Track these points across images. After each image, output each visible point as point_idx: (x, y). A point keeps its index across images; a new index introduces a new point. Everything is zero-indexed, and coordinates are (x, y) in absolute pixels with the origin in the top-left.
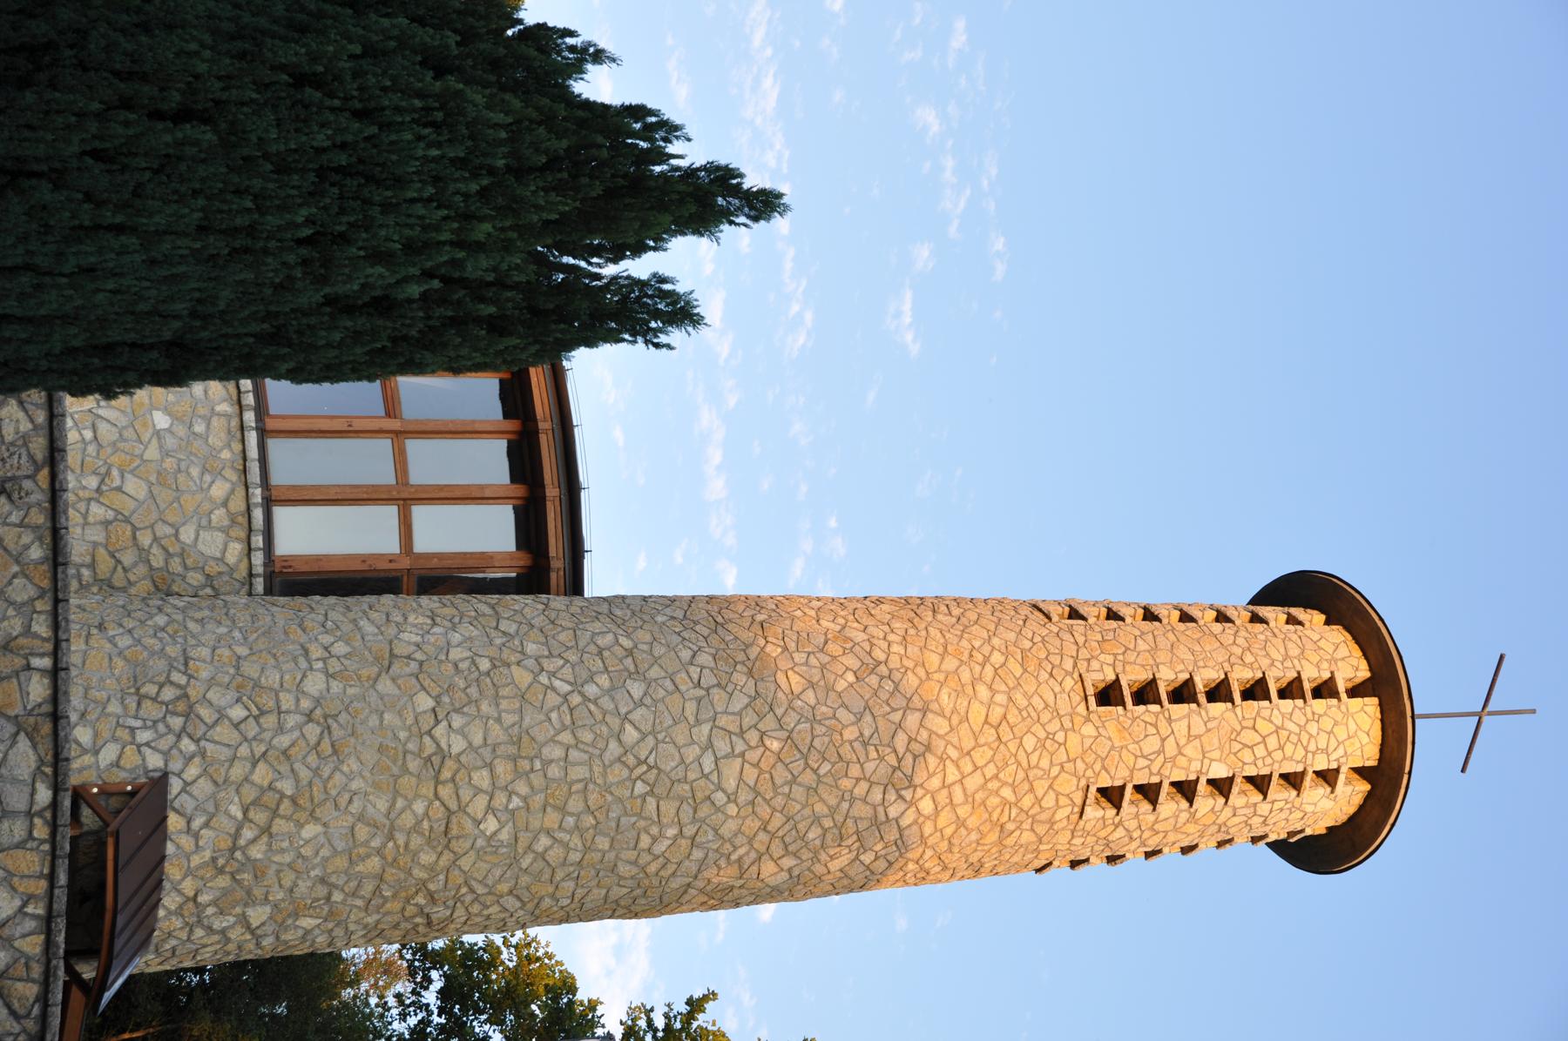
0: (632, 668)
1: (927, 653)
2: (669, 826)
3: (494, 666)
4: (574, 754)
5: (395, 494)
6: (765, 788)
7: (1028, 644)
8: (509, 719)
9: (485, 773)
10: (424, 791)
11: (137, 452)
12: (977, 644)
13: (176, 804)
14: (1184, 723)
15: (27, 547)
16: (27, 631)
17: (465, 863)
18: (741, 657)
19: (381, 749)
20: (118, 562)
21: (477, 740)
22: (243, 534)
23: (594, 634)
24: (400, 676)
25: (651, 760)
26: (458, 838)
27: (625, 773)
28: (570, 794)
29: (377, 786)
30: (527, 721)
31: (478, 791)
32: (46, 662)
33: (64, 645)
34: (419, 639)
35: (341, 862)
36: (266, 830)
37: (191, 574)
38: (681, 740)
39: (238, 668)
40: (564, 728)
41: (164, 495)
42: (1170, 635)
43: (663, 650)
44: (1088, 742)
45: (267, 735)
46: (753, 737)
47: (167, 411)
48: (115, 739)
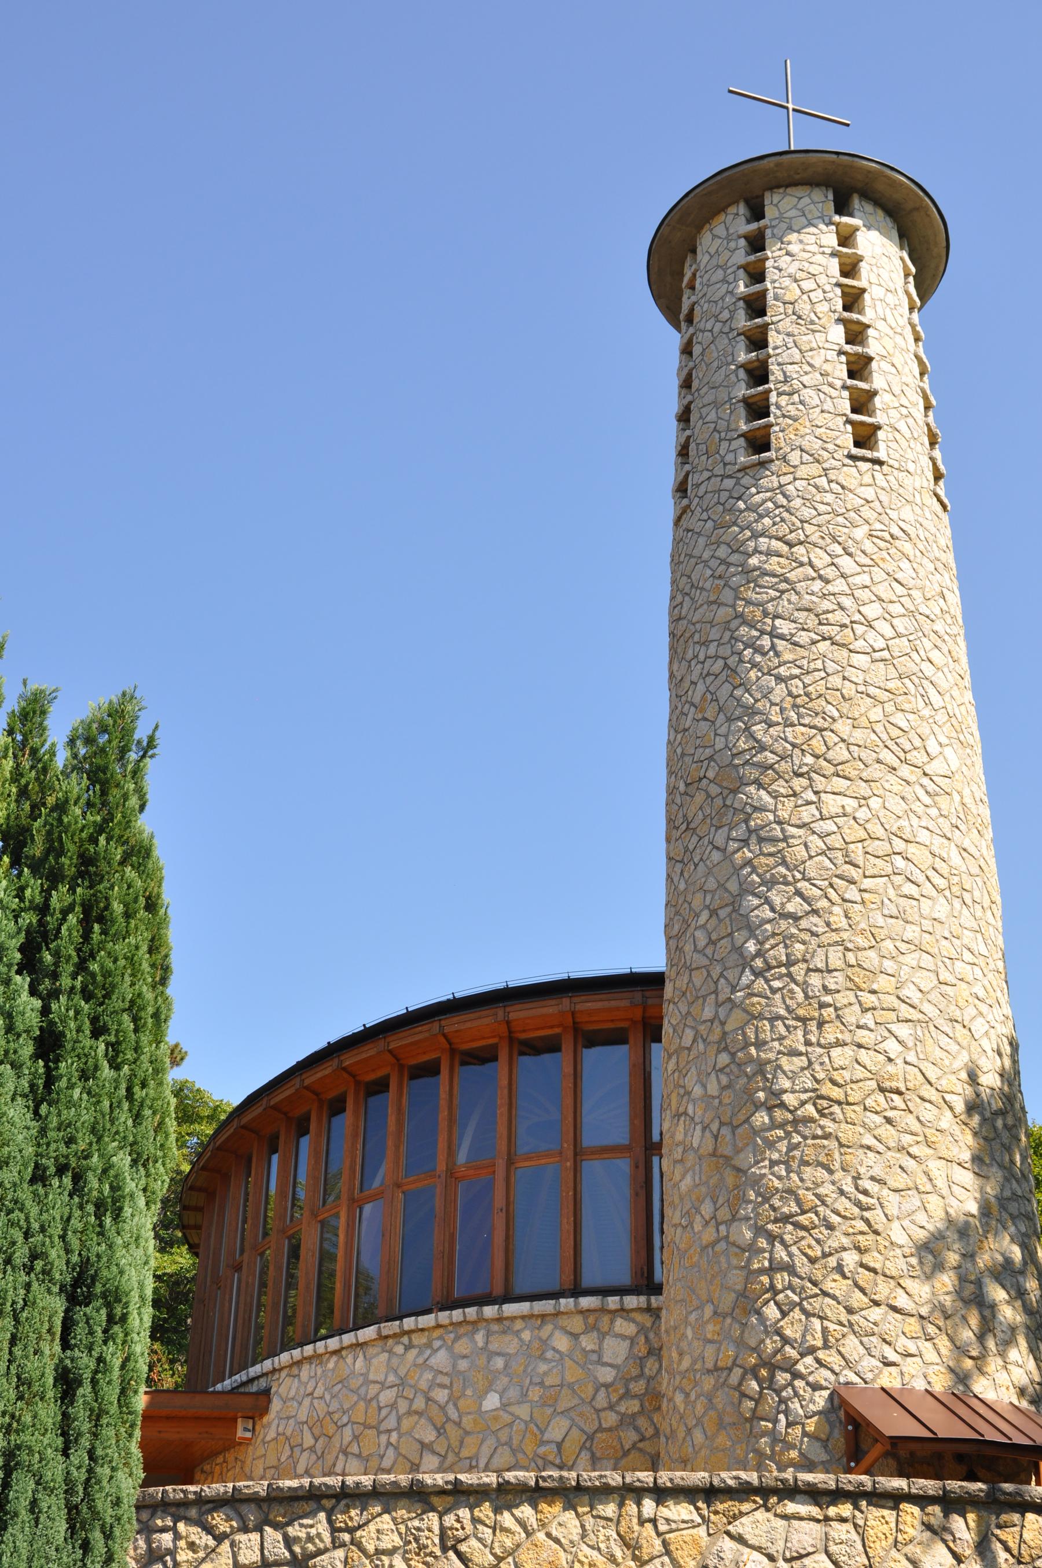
0: (729, 909)
1: (717, 620)
3: (726, 1049)
7: (710, 524)
11: (523, 1426)
12: (709, 572)
22: (606, 1319)
23: (696, 950)
24: (735, 1145)
32: (649, 1506)
34: (699, 1128)
37: (647, 1371)
42: (702, 392)
43: (711, 879)
47: (482, 1396)
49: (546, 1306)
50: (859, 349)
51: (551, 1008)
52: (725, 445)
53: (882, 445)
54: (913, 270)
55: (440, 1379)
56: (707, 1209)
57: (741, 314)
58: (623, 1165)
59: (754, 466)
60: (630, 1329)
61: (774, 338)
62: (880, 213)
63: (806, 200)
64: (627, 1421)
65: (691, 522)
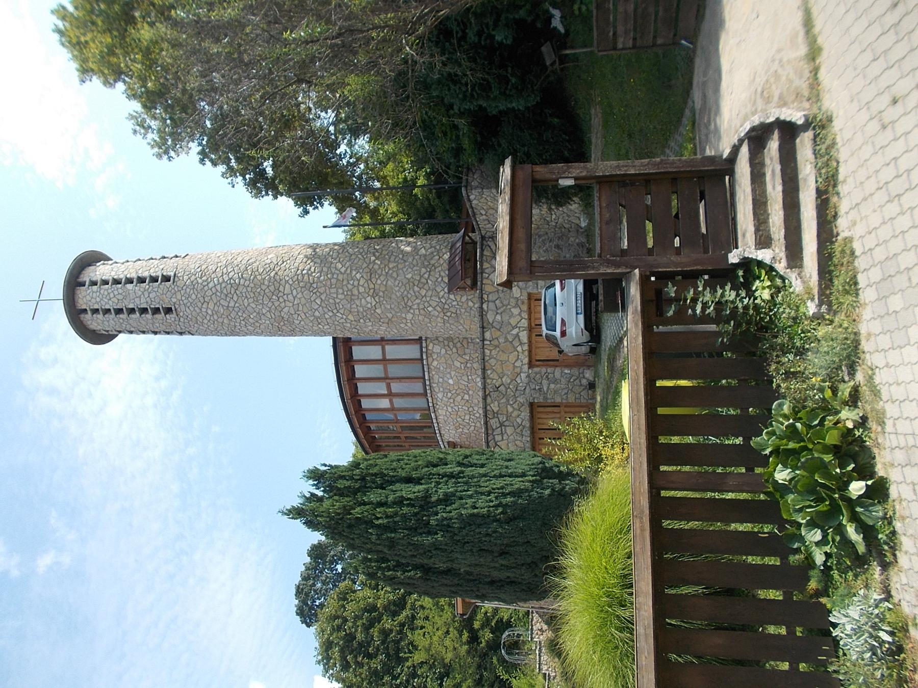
8: (354, 306)
16: (491, 351)
19: (391, 298)
32: (486, 342)
35: (400, 266)
36: (421, 277)
56: (402, 325)
57: (121, 316)
58: (387, 348)
61: (131, 306)
64: (455, 346)
65: (194, 331)
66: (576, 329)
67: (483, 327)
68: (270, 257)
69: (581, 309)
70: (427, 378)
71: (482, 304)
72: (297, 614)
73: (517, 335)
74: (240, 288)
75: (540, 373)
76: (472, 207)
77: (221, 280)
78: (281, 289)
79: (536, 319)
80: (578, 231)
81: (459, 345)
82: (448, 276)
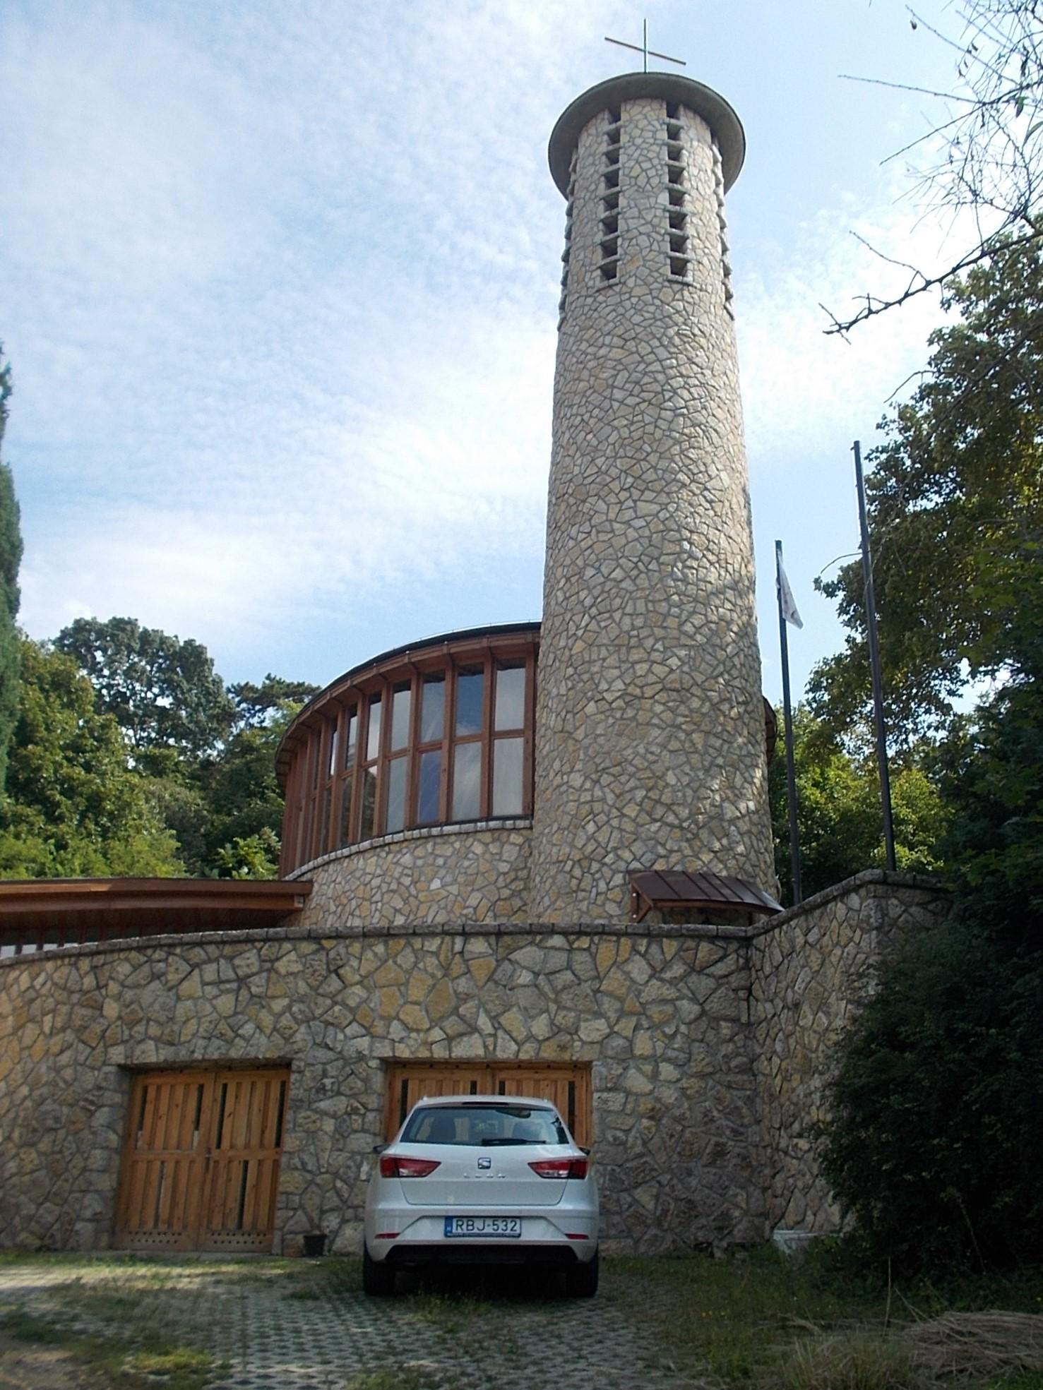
2: (681, 547)
4: (629, 609)
5: (486, 741)
6: (657, 486)
8: (604, 653)
9: (637, 667)
10: (648, 706)
13: (648, 865)
14: (630, 221)
15: (376, 954)
16: (436, 954)
17: (699, 678)
18: (574, 508)
19: (620, 735)
20: (520, 909)
21: (616, 672)
22: (506, 833)
25: (635, 560)
26: (681, 683)
27: (643, 576)
28: (655, 611)
29: (643, 737)
30: (605, 641)
31: (650, 671)
32: (459, 941)
33: (446, 928)
35: (695, 758)
36: (669, 807)
38: (624, 541)
39: (564, 829)
40: (611, 617)
41: (480, 882)
44: (639, 282)
45: (606, 808)
46: (624, 495)
48: (604, 905)
49: (469, 827)
50: (677, 208)
51: (474, 645)
52: (588, 275)
53: (690, 273)
54: (720, 158)
55: (406, 871)
57: (602, 185)
58: (519, 742)
59: (604, 288)
60: (520, 840)
61: (622, 201)
62: (698, 119)
63: (648, 108)
66: (403, 1214)
67: (499, 933)
68: (723, 475)
69: (464, 1235)
70: (447, 829)
71: (565, 933)
72: (77, 622)
73: (474, 1029)
74: (653, 411)
75: (368, 1090)
76: (825, 903)
77: (672, 372)
78: (649, 495)
79: (519, 1082)
80: (765, 1215)
81: (517, 903)
82: (670, 872)
